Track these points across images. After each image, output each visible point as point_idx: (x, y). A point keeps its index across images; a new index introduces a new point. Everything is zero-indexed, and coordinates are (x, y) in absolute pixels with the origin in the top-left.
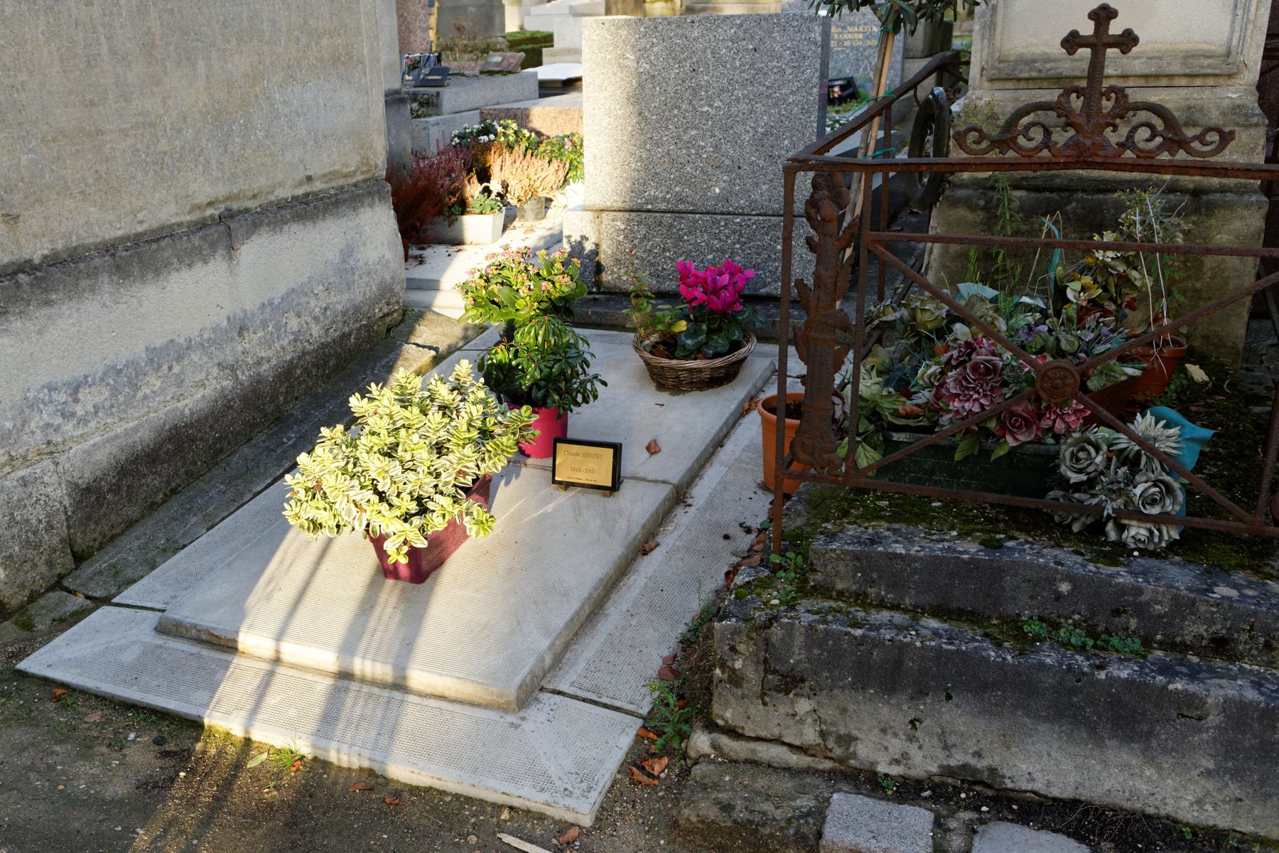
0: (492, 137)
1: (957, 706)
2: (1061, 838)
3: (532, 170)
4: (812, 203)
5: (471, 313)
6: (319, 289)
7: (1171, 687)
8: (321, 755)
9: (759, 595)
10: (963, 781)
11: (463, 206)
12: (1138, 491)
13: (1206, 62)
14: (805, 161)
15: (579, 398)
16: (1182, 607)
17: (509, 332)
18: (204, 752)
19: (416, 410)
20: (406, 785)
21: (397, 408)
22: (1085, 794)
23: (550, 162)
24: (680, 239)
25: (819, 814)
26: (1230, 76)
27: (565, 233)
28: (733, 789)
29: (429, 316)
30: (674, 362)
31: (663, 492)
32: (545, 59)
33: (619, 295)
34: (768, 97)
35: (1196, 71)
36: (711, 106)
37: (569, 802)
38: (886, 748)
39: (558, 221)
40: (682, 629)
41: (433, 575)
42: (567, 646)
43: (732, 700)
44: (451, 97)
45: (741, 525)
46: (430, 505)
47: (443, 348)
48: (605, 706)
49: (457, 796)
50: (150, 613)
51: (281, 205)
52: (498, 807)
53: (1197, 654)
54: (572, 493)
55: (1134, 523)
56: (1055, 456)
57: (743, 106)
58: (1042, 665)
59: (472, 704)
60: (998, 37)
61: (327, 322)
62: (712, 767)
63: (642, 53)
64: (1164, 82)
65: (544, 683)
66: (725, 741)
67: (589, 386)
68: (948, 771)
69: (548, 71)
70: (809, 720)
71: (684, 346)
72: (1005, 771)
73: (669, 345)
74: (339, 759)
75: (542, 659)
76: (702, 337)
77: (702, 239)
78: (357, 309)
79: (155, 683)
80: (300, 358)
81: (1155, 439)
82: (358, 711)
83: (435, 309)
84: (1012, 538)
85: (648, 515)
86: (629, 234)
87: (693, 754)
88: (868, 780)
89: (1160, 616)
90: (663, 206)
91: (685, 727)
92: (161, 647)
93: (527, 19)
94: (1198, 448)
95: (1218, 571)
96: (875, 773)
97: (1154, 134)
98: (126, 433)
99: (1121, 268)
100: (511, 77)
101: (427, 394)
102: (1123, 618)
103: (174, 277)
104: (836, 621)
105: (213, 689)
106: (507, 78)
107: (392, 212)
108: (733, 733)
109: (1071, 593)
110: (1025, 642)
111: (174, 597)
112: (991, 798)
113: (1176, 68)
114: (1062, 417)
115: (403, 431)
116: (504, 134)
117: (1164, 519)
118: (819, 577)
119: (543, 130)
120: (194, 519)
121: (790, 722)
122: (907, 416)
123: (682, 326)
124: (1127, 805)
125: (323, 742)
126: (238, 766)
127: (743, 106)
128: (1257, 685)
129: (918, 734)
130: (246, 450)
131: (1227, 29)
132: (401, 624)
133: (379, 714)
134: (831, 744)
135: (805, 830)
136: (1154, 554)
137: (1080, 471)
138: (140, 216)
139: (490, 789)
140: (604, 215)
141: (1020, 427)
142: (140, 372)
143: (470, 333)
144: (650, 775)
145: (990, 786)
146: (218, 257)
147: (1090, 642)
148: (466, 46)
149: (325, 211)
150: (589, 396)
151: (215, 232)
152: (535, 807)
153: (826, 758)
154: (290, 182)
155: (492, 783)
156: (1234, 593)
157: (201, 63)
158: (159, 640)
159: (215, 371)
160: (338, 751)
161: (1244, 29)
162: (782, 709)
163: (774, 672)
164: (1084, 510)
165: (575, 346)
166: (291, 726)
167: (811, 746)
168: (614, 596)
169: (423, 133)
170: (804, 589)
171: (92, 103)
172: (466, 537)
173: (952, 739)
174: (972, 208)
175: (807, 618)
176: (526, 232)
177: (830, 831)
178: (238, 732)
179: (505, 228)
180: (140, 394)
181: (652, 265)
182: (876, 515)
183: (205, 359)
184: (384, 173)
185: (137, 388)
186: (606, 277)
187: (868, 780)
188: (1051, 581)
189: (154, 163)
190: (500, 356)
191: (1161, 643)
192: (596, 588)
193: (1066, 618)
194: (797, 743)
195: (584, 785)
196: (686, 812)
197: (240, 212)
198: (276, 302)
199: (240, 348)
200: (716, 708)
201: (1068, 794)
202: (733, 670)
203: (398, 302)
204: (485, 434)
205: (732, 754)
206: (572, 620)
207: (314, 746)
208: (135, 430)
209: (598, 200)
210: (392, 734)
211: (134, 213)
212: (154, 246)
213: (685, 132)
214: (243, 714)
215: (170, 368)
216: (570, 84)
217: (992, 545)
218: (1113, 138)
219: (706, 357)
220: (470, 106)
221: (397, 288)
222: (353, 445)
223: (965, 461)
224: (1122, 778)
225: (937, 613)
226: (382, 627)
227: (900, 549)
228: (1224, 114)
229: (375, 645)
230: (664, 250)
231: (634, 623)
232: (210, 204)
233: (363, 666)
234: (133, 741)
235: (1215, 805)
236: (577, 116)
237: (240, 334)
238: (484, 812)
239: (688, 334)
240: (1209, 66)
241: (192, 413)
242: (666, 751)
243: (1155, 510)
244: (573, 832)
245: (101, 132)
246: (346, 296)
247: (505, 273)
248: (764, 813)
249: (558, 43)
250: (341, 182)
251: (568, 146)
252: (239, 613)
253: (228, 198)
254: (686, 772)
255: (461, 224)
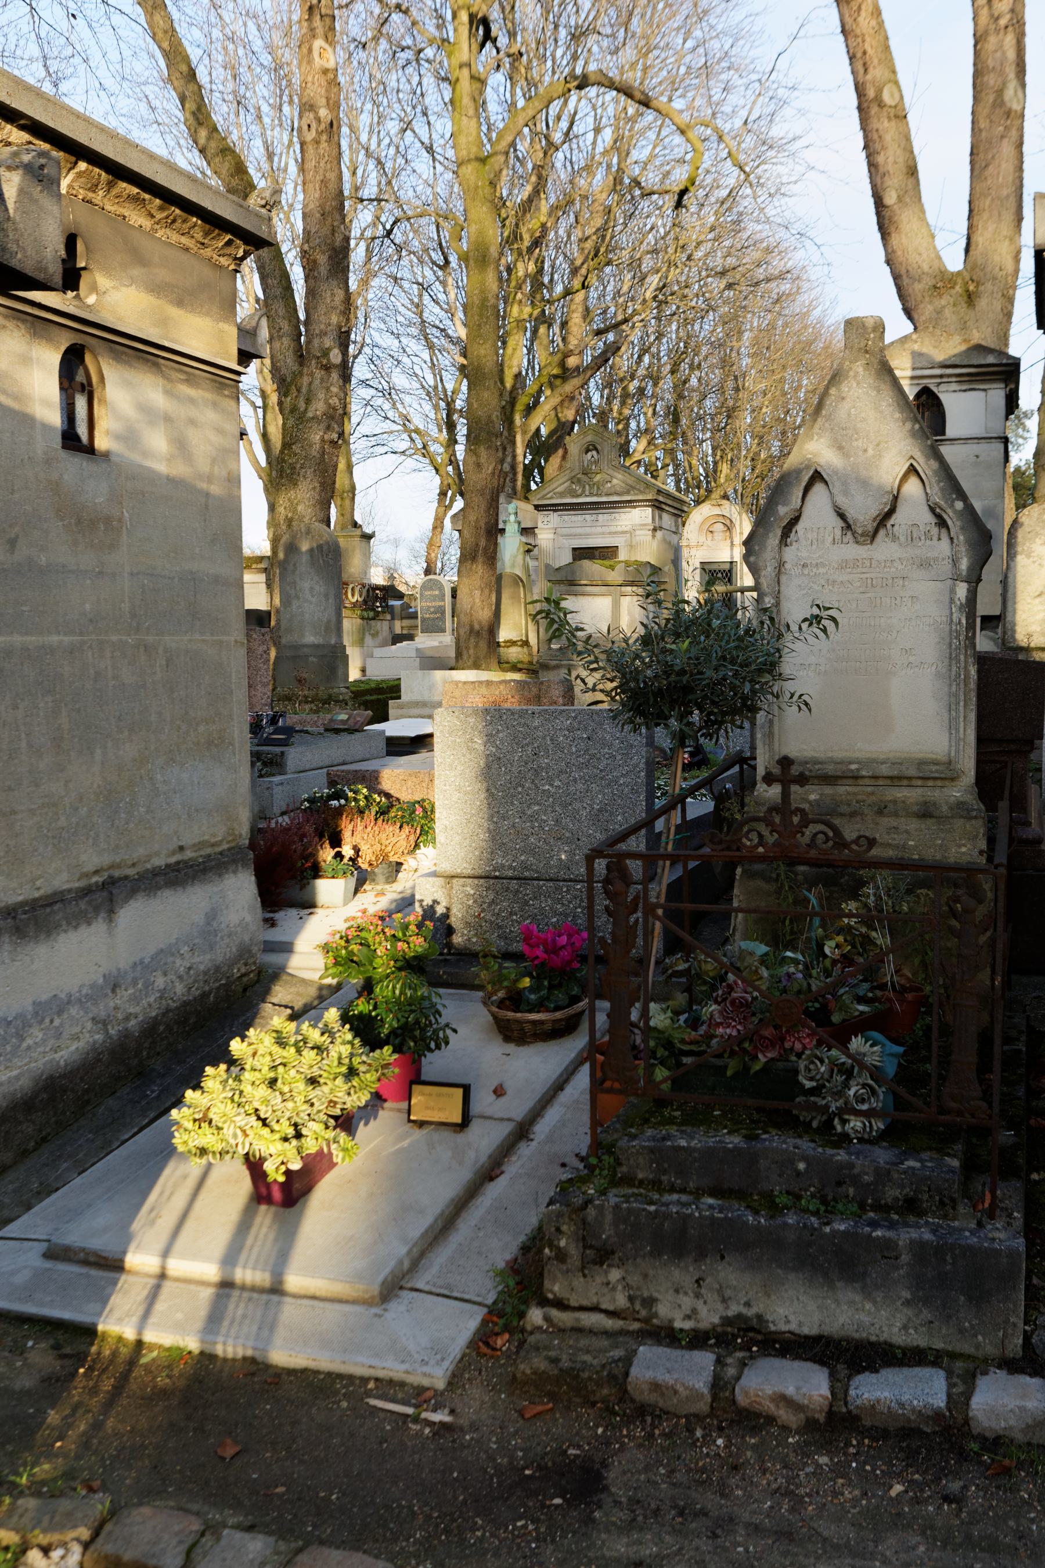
0: (343, 802)
1: (730, 1264)
2: (809, 1365)
3: (383, 836)
4: (607, 881)
5: (331, 971)
6: (185, 949)
7: (874, 1234)
8: (208, 1349)
9: (579, 1188)
10: (739, 1329)
11: (316, 872)
12: (852, 1092)
13: (934, 768)
14: (601, 852)
15: (433, 1045)
16: (883, 1176)
17: (368, 988)
18: (99, 1353)
19: (293, 1050)
20: (283, 1369)
21: (276, 1049)
22: (827, 1330)
23: (401, 827)
24: (526, 903)
25: (628, 1361)
26: (953, 779)
27: (418, 897)
28: (560, 1349)
29: (284, 977)
30: (519, 1015)
31: (506, 1128)
32: (392, 712)
33: (467, 956)
34: (602, 778)
35: (928, 774)
36: (552, 785)
37: (425, 1369)
38: (680, 1306)
39: (409, 884)
40: (522, 1238)
41: (302, 1201)
42: (422, 1254)
43: (559, 1275)
44: (296, 756)
45: (577, 1155)
46: (304, 1132)
47: (298, 1005)
48: (456, 1299)
49: (329, 1374)
50: (36, 1244)
51: (156, 872)
52: (365, 1380)
53: (897, 1213)
54: (425, 1131)
55: (852, 1117)
56: (797, 1072)
57: (580, 786)
58: (786, 1224)
59: (340, 1301)
60: (776, 744)
61: (190, 981)
62: (544, 1336)
63: (490, 738)
64: (905, 782)
65: (403, 1283)
66: (554, 1313)
67: (441, 1034)
68: (726, 1321)
69: (396, 727)
70: (620, 1287)
71: (528, 1000)
72: (769, 1317)
73: (515, 1000)
74: (225, 1351)
75: (401, 1262)
76: (544, 992)
77: (546, 904)
78: (217, 969)
79: (48, 1299)
80: (164, 1014)
81: (864, 1055)
82: (240, 1312)
83: (290, 971)
84: (766, 1132)
85: (494, 1146)
86: (479, 901)
87: (529, 1328)
88: (667, 1336)
89: (869, 1185)
90: (510, 873)
91: (523, 1307)
92: (49, 1269)
93: (369, 661)
94: (896, 1061)
95: (913, 1152)
96: (672, 1329)
97: (828, 839)
98: (10, 1081)
99: (864, 930)
100: (358, 735)
101: (300, 1038)
102: (844, 1188)
103: (62, 938)
104: (636, 1201)
105: (105, 1300)
106: (353, 736)
107: (253, 878)
108: (561, 1305)
109: (806, 1169)
110: (775, 1210)
111: (57, 1230)
112: (761, 1342)
113: (912, 772)
114: (799, 1039)
115: (281, 1069)
116: (355, 799)
117: (869, 1114)
118: (624, 1169)
119: (392, 792)
120: (65, 1165)
121: (605, 1290)
122: (691, 1043)
123: (526, 982)
124: (856, 1336)
125: (210, 1338)
126: (132, 1362)
127: (580, 786)
128: (934, 1232)
129: (703, 1291)
130: (110, 1102)
131: (947, 744)
132: (276, 1240)
133: (259, 1313)
134: (638, 1307)
135: (616, 1371)
136: (870, 1142)
137: (811, 1079)
138: (38, 883)
139: (357, 1365)
140: (455, 881)
141: (767, 1047)
142: (26, 1024)
143: (325, 992)
144: (494, 1349)
145: (759, 1332)
146: (100, 920)
147: (823, 1208)
148: (306, 697)
149: (194, 878)
150: (441, 1043)
151: (99, 897)
152: (397, 1376)
153: (635, 1320)
154: (164, 852)
155: (360, 1359)
156: (918, 1165)
157: (99, 751)
158: (48, 1264)
159: (89, 1025)
160: (225, 1344)
161: (957, 744)
162: (599, 1279)
163: (591, 1247)
164: (815, 1107)
165: (429, 998)
166: (179, 1327)
167: (623, 1311)
168: (464, 1215)
169: (267, 793)
170: (616, 1182)
171: (10, 789)
172: (332, 1165)
173: (728, 1293)
174: (767, 880)
175: (613, 1200)
176: (377, 895)
177: (634, 1371)
178: (130, 1334)
179: (356, 892)
180: (25, 1045)
181: (500, 927)
182: (671, 1121)
183: (82, 1013)
184: (247, 842)
185: (22, 1039)
186: (457, 939)
187: (667, 1336)
188: (792, 1162)
189: (54, 837)
190: (361, 1008)
191: (871, 1206)
192: (447, 1207)
193: (806, 1190)
194: (611, 1308)
195: (438, 1357)
196: (522, 1367)
197: (120, 879)
198: (147, 961)
199: (112, 1004)
200: (547, 1284)
201: (814, 1331)
202: (559, 1248)
203: (255, 963)
204: (352, 1073)
205: (560, 1324)
206: (427, 1231)
207: (202, 1341)
208: (17, 1078)
209: (446, 867)
210: (272, 1328)
211: (33, 881)
212: (48, 910)
213: (529, 807)
214: (135, 1319)
215: (52, 1021)
216: (421, 743)
217: (750, 1138)
218: (805, 839)
219: (548, 1010)
220: (314, 765)
221: (255, 949)
222: (238, 1079)
223: (736, 1075)
224: (850, 1314)
225: (712, 1194)
226: (259, 1243)
227: (683, 1143)
228: (951, 808)
229: (253, 1257)
230: (511, 914)
231: (481, 1234)
232: (96, 872)
233: (243, 1275)
234: (32, 1347)
235: (916, 1329)
236: (427, 779)
237: (113, 991)
238: (352, 1384)
239: (531, 989)
240: (937, 771)
241: (66, 1065)
242: (506, 1328)
243: (865, 1107)
244: (429, 1394)
245: (14, 812)
246: (208, 957)
247: (363, 934)
248: (585, 1362)
249: (406, 695)
250: (209, 851)
251: (419, 812)
252: (126, 1238)
253: (112, 867)
254: (522, 1343)
255: (314, 888)
